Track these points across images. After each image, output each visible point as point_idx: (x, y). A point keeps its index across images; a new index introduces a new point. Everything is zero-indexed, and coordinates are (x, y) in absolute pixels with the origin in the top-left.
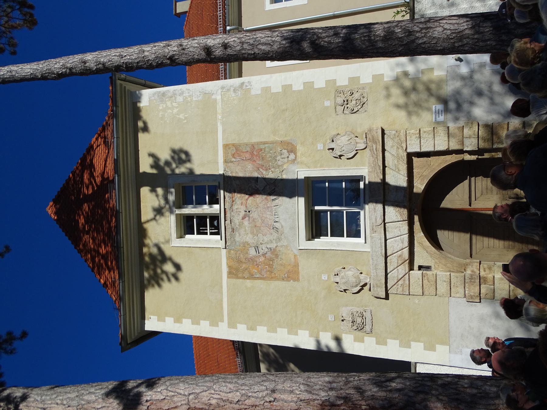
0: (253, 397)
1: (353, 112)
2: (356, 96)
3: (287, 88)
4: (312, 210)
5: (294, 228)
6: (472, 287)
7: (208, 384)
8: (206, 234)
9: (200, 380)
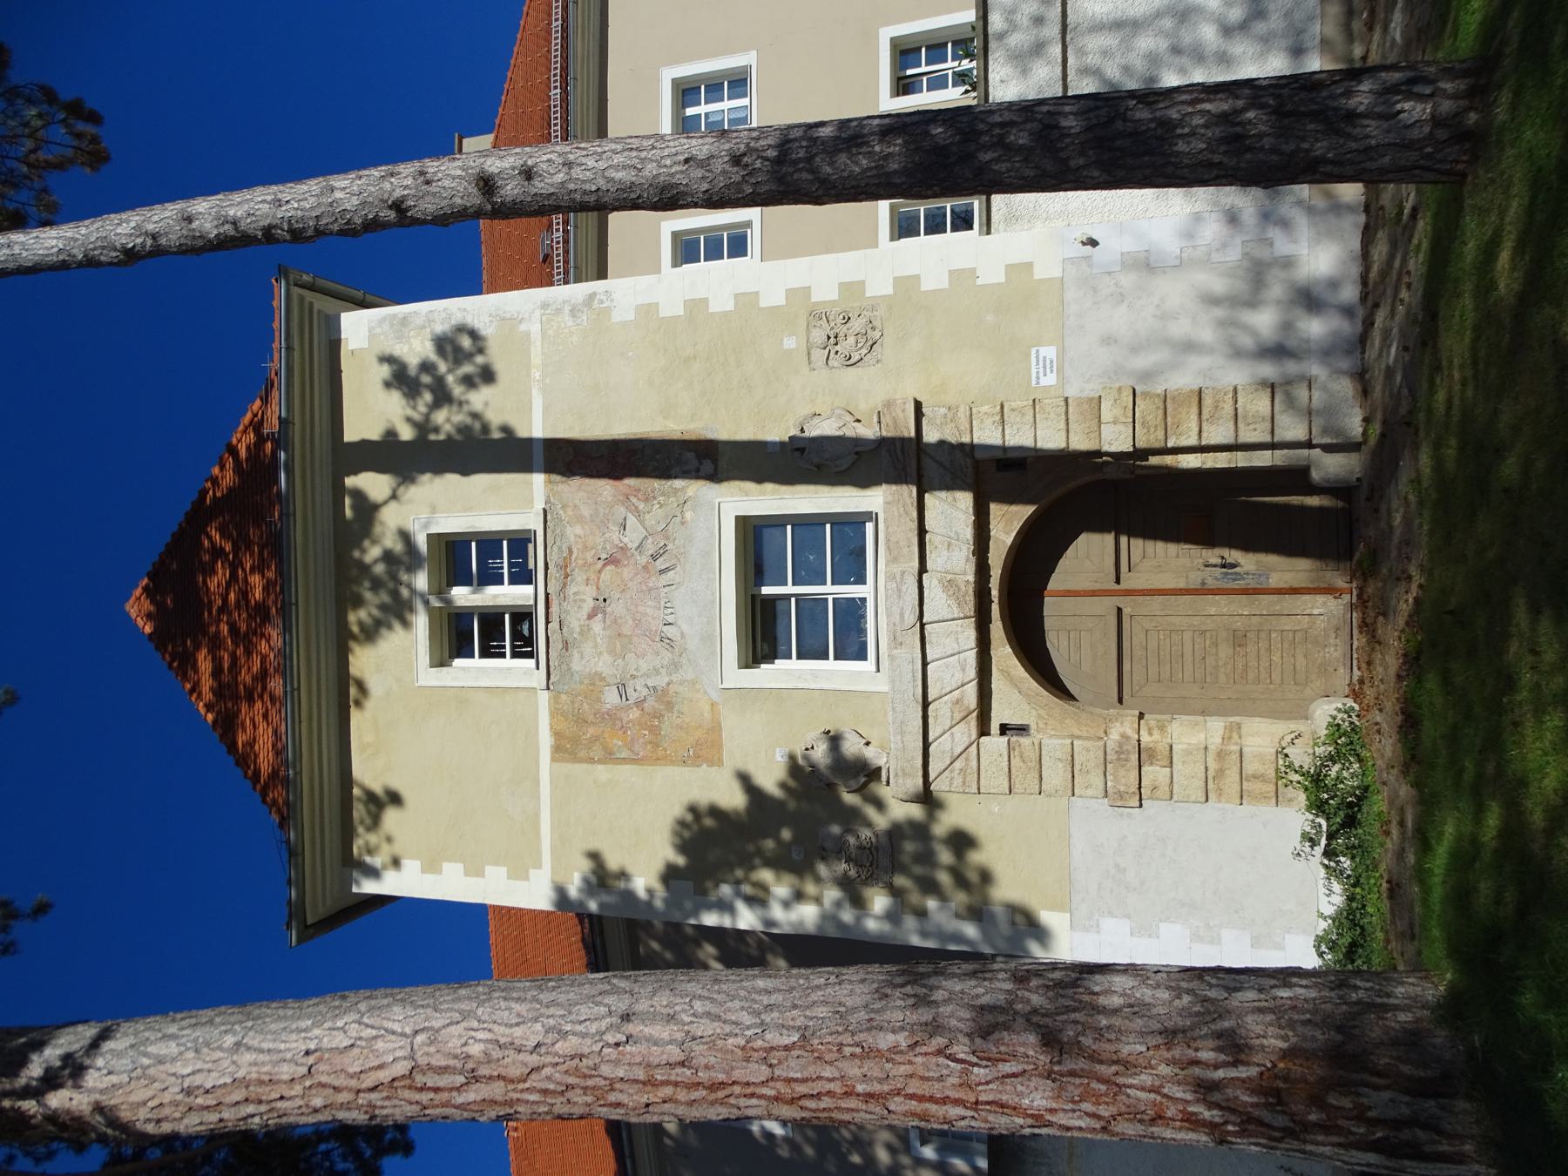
0: (574, 1034)
1: (849, 362)
2: (857, 325)
3: (696, 307)
4: (753, 597)
5: (712, 639)
6: (1122, 772)
7: (465, 1006)
8: (503, 655)
9: (445, 995)
